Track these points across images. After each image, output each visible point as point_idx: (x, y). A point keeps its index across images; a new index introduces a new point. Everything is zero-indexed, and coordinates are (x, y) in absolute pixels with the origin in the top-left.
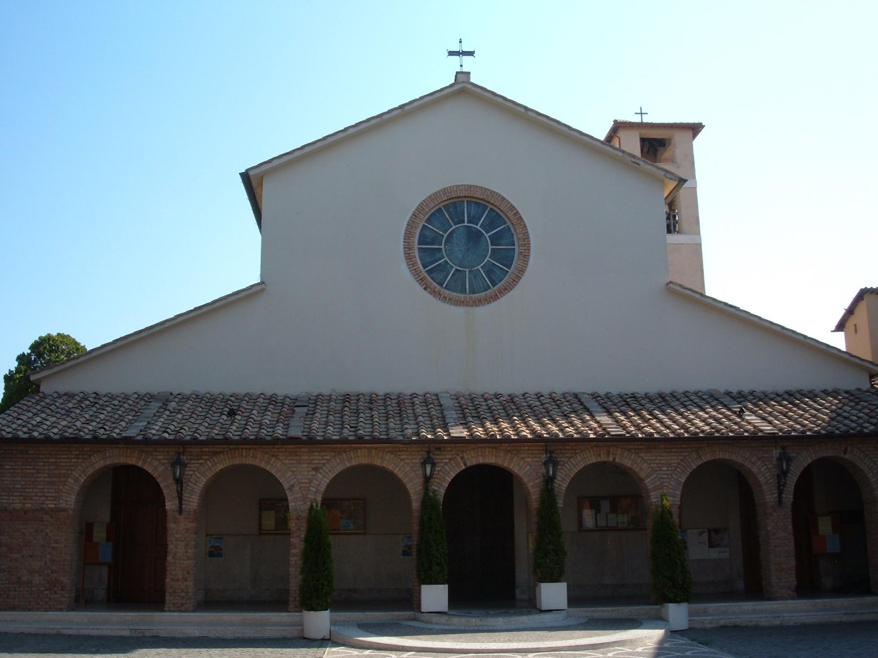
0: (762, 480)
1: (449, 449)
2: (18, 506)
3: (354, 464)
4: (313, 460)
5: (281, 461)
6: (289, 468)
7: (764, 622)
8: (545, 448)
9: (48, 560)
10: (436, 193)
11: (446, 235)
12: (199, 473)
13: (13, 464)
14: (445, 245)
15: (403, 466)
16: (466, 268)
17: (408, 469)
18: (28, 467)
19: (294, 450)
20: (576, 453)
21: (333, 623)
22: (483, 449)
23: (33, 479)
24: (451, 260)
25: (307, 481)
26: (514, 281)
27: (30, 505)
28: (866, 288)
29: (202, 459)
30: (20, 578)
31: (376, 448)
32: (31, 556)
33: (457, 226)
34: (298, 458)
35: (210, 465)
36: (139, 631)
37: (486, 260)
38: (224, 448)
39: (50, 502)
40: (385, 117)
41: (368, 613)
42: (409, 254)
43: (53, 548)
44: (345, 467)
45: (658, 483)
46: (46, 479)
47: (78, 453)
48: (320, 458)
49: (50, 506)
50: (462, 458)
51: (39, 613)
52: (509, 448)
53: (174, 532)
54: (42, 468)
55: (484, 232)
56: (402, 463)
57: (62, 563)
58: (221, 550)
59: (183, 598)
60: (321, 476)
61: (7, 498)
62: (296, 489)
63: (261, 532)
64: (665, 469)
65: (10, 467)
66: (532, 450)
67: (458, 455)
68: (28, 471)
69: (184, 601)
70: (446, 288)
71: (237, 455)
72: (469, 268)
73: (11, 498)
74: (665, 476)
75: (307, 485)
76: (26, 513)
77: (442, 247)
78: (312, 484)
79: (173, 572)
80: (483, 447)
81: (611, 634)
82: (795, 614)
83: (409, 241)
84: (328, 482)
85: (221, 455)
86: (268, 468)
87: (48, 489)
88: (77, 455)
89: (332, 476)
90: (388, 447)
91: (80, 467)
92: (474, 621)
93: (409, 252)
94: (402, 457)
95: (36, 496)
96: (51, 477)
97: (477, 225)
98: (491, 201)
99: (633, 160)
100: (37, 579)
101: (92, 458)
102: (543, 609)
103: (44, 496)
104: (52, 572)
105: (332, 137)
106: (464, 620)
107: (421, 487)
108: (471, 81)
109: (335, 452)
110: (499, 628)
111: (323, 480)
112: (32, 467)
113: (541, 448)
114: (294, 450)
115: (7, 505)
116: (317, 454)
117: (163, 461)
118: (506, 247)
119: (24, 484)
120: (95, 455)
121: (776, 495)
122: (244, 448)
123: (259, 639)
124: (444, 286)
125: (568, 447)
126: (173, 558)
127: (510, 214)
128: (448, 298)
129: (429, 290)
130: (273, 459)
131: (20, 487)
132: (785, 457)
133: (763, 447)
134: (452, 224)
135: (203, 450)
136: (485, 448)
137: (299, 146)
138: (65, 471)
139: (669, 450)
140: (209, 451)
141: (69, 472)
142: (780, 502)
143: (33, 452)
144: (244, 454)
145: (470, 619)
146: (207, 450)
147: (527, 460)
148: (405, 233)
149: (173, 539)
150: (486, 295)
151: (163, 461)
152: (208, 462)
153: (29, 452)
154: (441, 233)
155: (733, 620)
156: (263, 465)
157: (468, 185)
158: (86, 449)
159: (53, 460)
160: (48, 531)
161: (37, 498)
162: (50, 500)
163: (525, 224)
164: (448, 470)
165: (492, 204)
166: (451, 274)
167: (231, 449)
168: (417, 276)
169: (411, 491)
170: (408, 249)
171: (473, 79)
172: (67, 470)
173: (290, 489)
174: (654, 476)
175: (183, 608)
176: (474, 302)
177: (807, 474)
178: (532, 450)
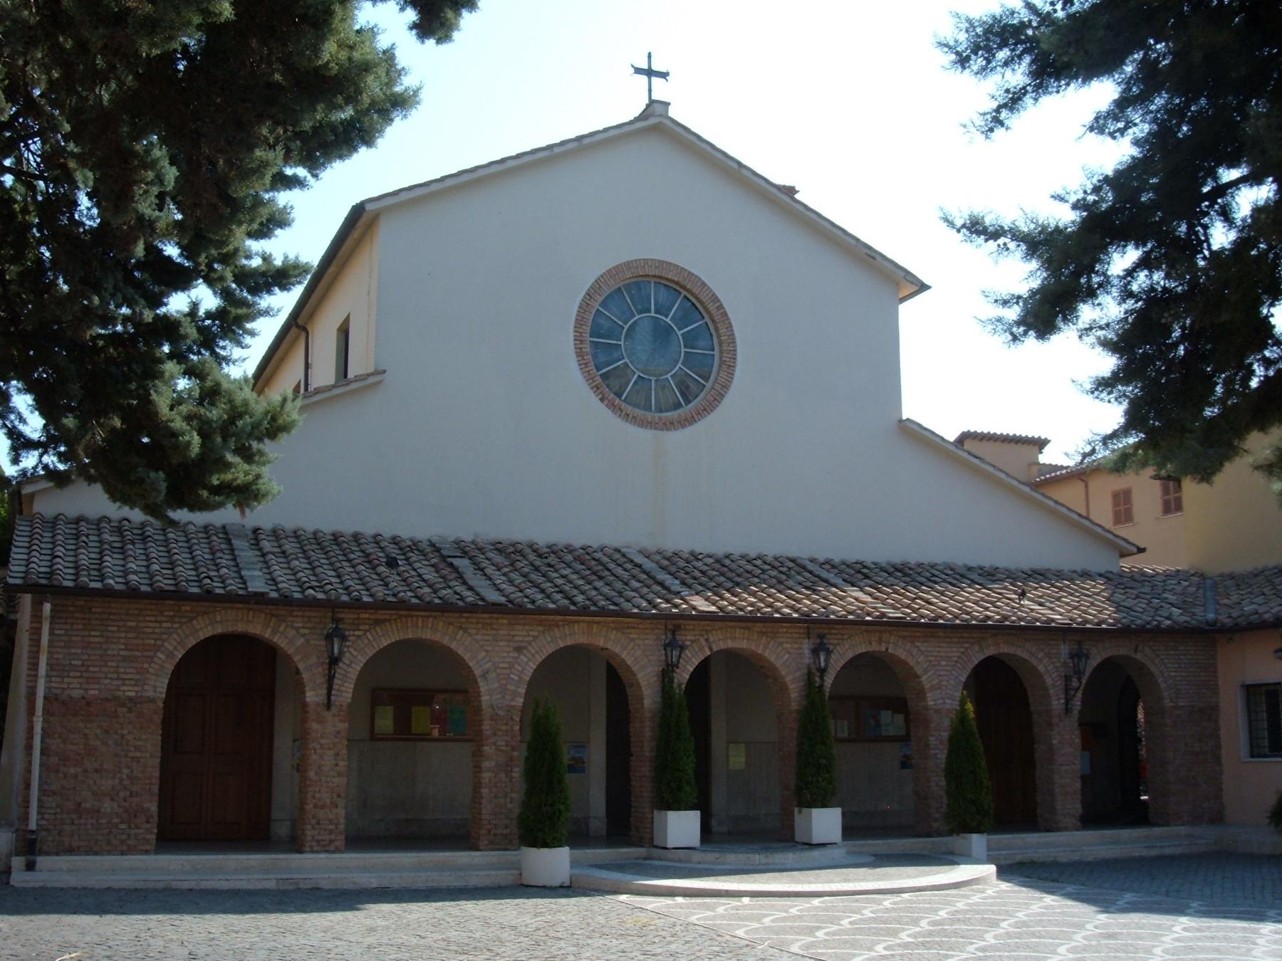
0: (1049, 681)
1: (691, 627)
2: (77, 693)
3: (569, 643)
4: (516, 636)
5: (470, 635)
6: (482, 646)
7: (1063, 857)
8: (806, 631)
9: (125, 777)
10: (617, 266)
11: (626, 327)
12: (355, 650)
13: (68, 627)
14: (625, 341)
15: (633, 648)
16: (650, 375)
17: (639, 653)
18: (93, 633)
19: (488, 621)
20: (843, 639)
21: (574, 863)
22: (733, 630)
23: (102, 652)
24: (631, 362)
25: (506, 665)
26: (715, 399)
27: (97, 692)
28: (969, 431)
29: (359, 630)
30: (79, 805)
31: (598, 623)
32: (97, 771)
33: (642, 315)
34: (495, 632)
35: (371, 639)
36: (292, 881)
37: (677, 368)
38: (391, 615)
39: (130, 688)
40: (557, 150)
41: (588, 851)
42: (581, 348)
43: (133, 758)
44: (558, 648)
45: (935, 682)
46: (122, 653)
47: (172, 613)
48: (525, 633)
49: (128, 694)
50: (707, 640)
51: (112, 857)
52: (763, 630)
53: (319, 735)
54: (116, 635)
55: (675, 328)
56: (632, 644)
57: (148, 782)
58: (583, 762)
59: (331, 832)
60: (526, 660)
61: (60, 680)
62: (492, 676)
63: (374, 737)
64: (944, 663)
65: (62, 632)
66: (792, 633)
67: (702, 636)
68: (92, 639)
69: (333, 837)
70: (625, 401)
71: (409, 624)
72: (655, 376)
73: (66, 680)
74: (944, 673)
75: (507, 671)
76: (88, 704)
77: (621, 343)
78: (513, 670)
79: (317, 795)
80: (731, 627)
81: (938, 873)
82: (1095, 848)
83: (581, 330)
84: (535, 667)
85: (387, 624)
86: (453, 646)
87: (125, 668)
88: (170, 616)
89: (539, 659)
90: (613, 622)
91: (175, 636)
92: (758, 858)
93: (582, 346)
94: (632, 636)
95: (106, 678)
96: (130, 650)
97: (667, 317)
98: (688, 287)
99: (868, 251)
100: (107, 806)
101: (195, 622)
102: (815, 841)
103: (118, 679)
104: (131, 795)
105: (483, 170)
106: (742, 857)
107: (656, 678)
108: (670, 114)
109: (544, 626)
110: (788, 866)
111: (528, 665)
112: (98, 633)
113: (802, 631)
114: (488, 621)
115: (58, 691)
116: (520, 627)
117: (302, 631)
118: (704, 352)
119: (86, 660)
120: (200, 618)
121: (1063, 701)
122: (420, 616)
123: (436, 889)
124: (623, 398)
125: (833, 631)
126: (316, 773)
127: (712, 307)
128: (631, 416)
129: (606, 402)
130: (461, 632)
131: (80, 663)
132: (1078, 655)
133: (1050, 640)
134: (635, 313)
135: (361, 616)
136: (735, 627)
137: (438, 177)
138: (153, 642)
139: (948, 640)
140: (369, 619)
141: (159, 642)
142: (1068, 710)
143: (99, 610)
144: (420, 625)
145: (751, 856)
146: (367, 616)
147: (786, 646)
148: (577, 319)
149: (318, 746)
150: (679, 415)
151: (302, 631)
152: (368, 634)
153: (94, 610)
154: (621, 323)
155: (1029, 855)
156: (445, 641)
157: (659, 261)
158: (183, 608)
159: (133, 624)
160: (125, 732)
161: (108, 681)
162: (129, 685)
163: (730, 323)
164: (690, 655)
165: (687, 290)
166: (633, 382)
167: (401, 617)
168: (591, 381)
169: (643, 683)
170: (578, 342)
171: (673, 113)
172: (156, 640)
173: (484, 675)
174: (932, 672)
175: (332, 848)
176: (664, 424)
177: (704, 667)
178: (792, 633)
